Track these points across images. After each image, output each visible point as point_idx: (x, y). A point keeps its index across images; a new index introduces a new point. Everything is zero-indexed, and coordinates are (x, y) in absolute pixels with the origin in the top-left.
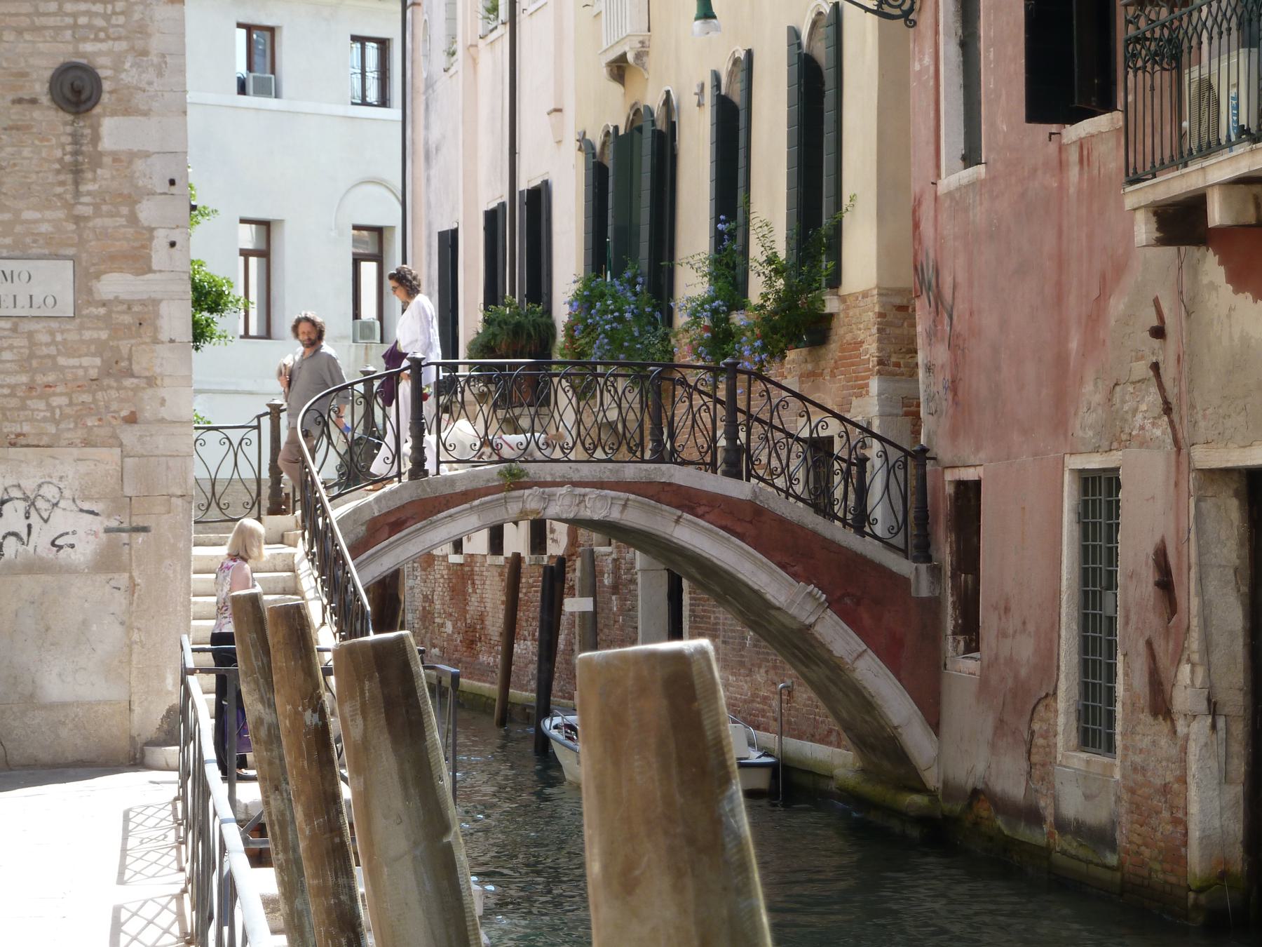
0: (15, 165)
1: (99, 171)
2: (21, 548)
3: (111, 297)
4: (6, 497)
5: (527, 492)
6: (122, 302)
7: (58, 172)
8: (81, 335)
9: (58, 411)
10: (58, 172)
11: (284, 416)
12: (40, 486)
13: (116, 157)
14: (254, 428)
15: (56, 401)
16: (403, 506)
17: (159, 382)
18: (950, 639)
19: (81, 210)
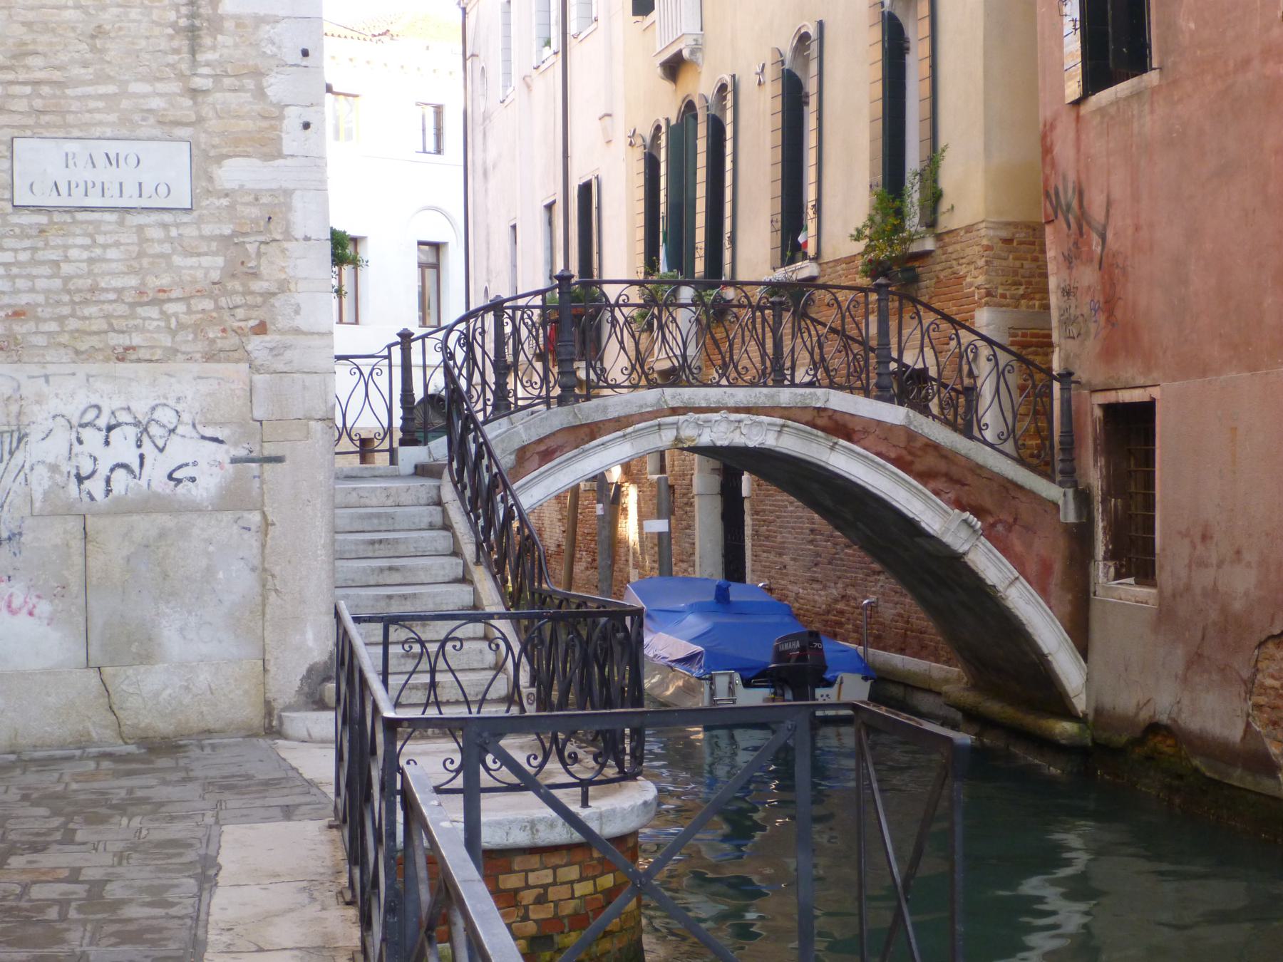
0: (120, 29)
1: (219, 37)
2: (132, 482)
3: (235, 185)
4: (113, 422)
5: (682, 418)
6: (248, 192)
7: (171, 37)
8: (199, 229)
9: (173, 321)
10: (171, 37)
11: (416, 347)
12: (153, 409)
13: (240, 22)
14: (385, 357)
15: (171, 308)
16: (553, 434)
17: (292, 287)
18: (1101, 565)
19: (198, 82)
